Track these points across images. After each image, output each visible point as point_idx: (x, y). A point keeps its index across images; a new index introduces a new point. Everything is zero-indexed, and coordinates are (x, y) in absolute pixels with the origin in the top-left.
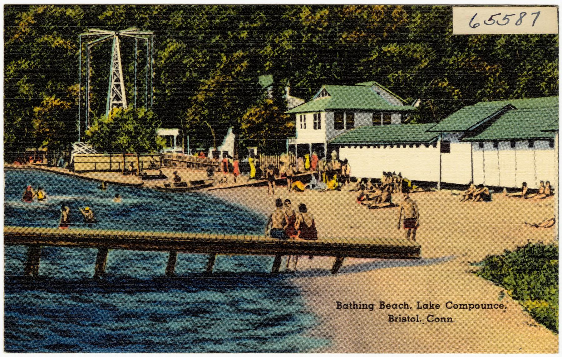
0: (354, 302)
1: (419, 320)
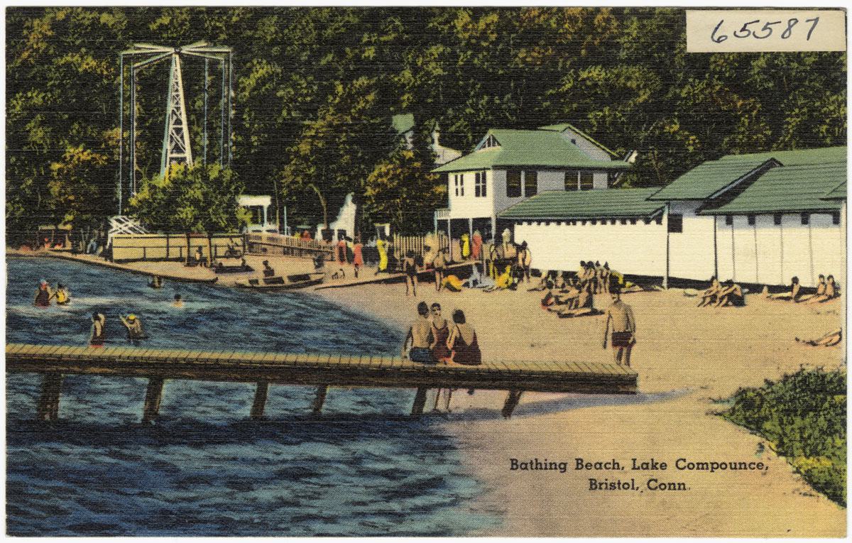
1: (635, 486)
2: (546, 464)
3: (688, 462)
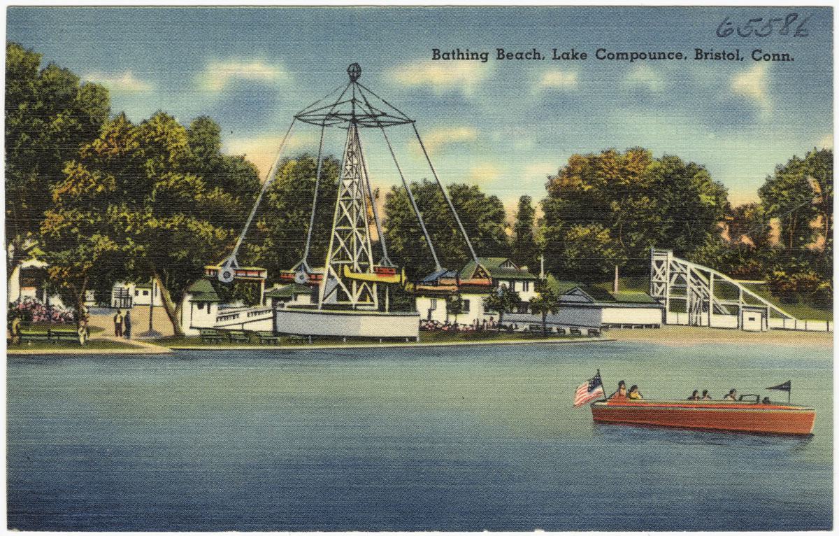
0: (458, 50)
1: (740, 57)
2: (467, 54)
3: (607, 52)
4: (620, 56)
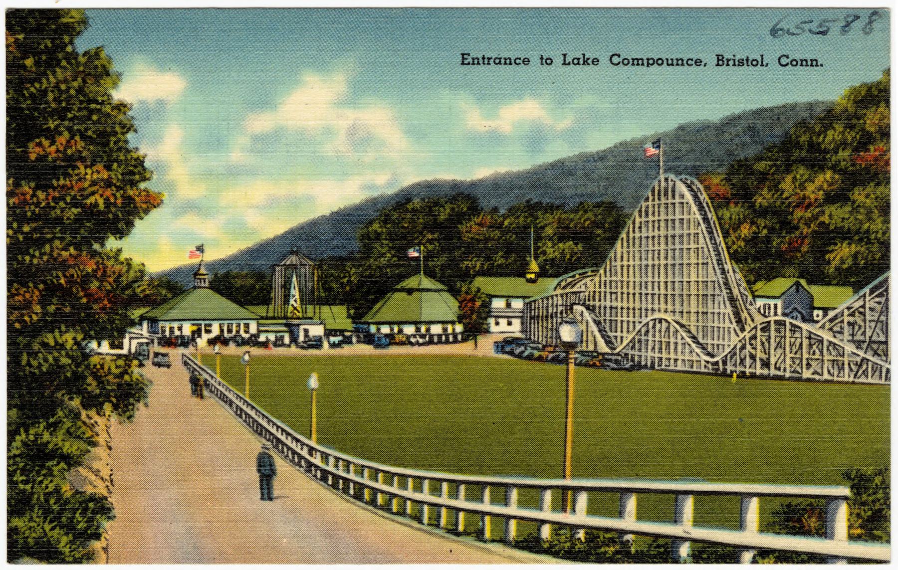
1: (765, 63)
3: (622, 58)
4: (636, 62)
